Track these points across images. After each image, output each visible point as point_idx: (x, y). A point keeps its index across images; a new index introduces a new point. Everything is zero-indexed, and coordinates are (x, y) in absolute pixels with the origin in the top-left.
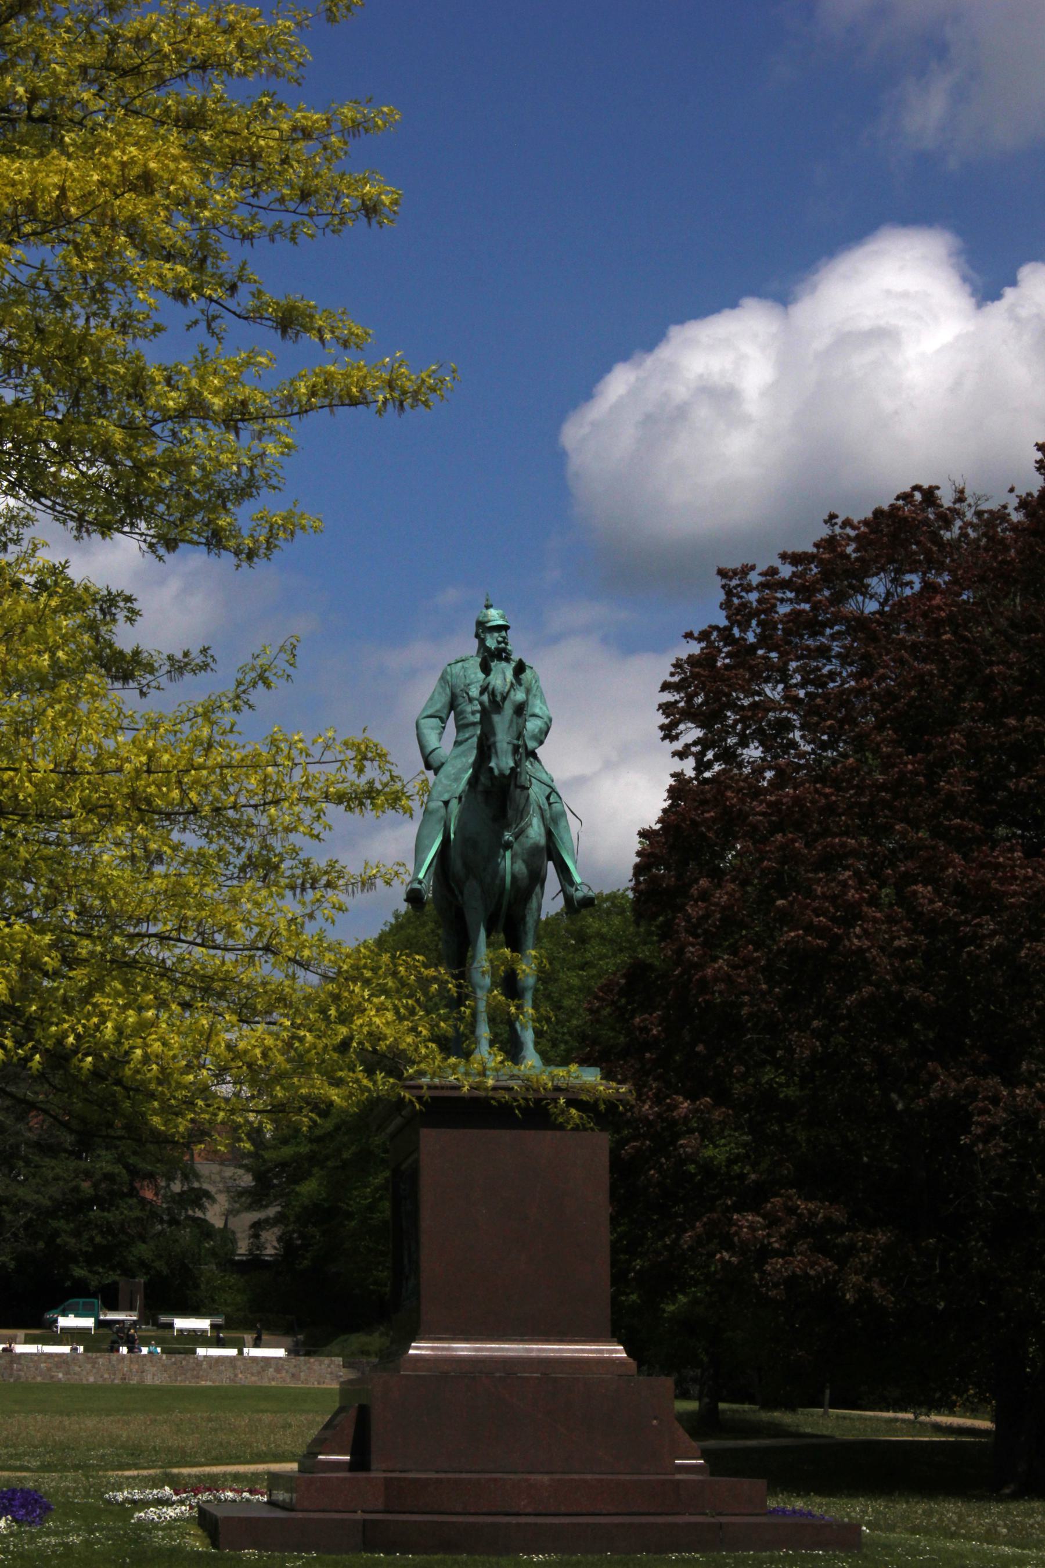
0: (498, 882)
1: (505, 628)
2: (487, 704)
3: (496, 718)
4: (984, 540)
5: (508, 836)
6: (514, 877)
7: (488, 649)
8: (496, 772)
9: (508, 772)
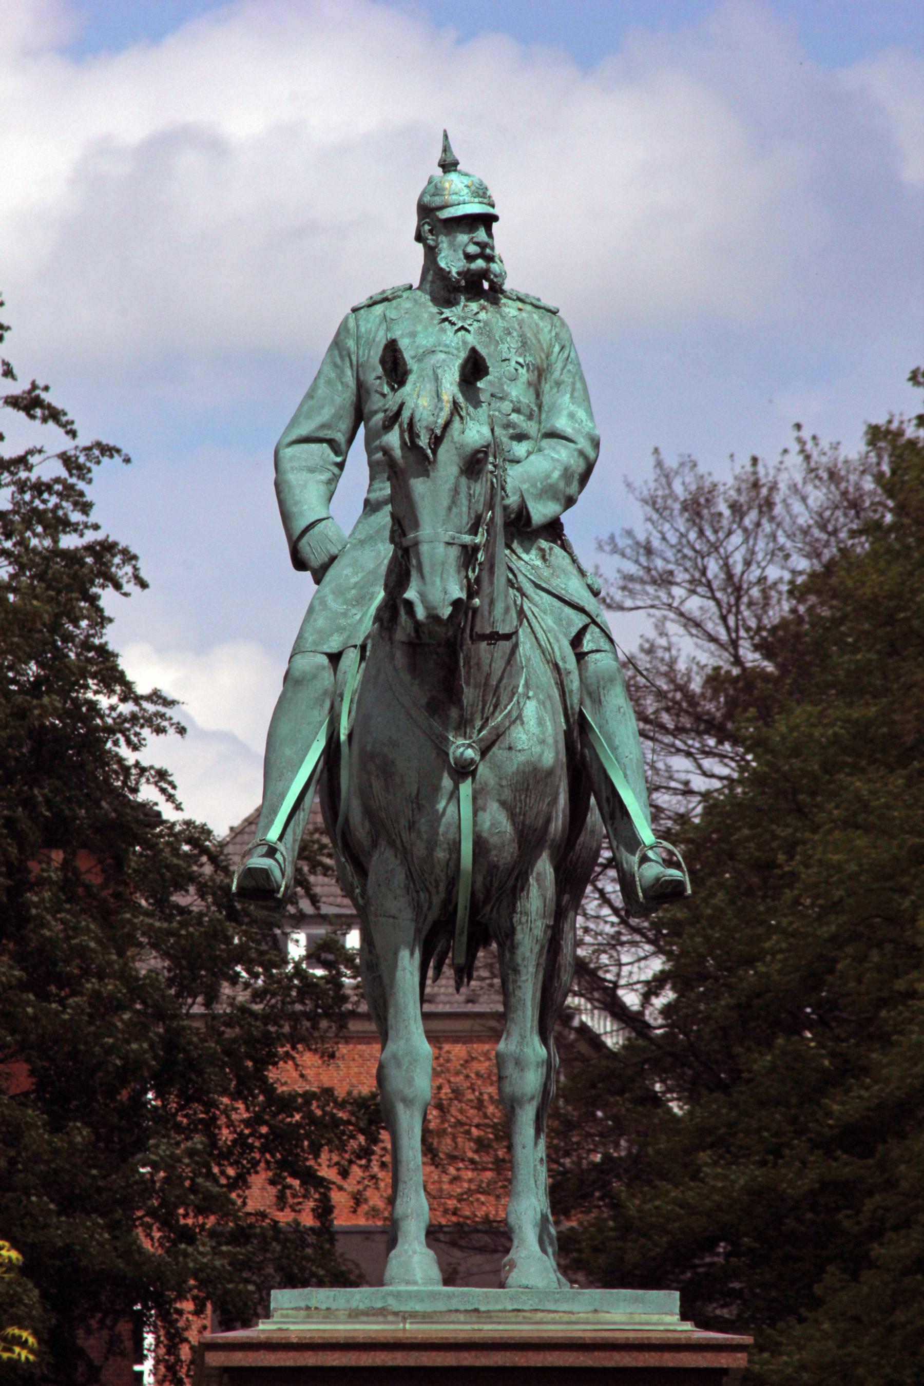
0: (441, 854)
1: (487, 221)
2: (398, 453)
3: (418, 486)
4: (67, 1178)
5: (462, 748)
6: (479, 843)
7: (442, 275)
8: (421, 613)
9: (446, 612)
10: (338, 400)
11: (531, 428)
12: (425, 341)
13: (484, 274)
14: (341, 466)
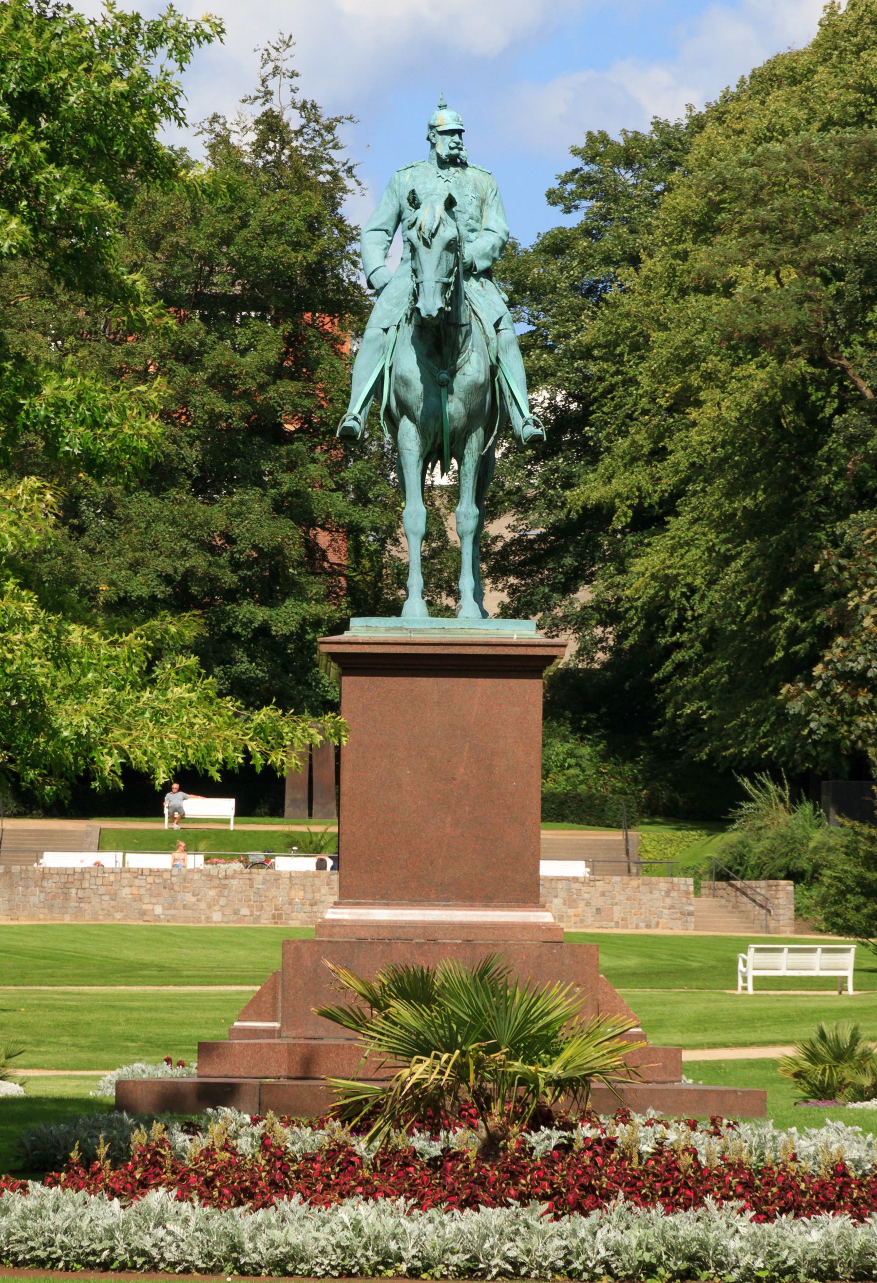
1: (459, 132)
12: (430, 186)
13: (457, 156)
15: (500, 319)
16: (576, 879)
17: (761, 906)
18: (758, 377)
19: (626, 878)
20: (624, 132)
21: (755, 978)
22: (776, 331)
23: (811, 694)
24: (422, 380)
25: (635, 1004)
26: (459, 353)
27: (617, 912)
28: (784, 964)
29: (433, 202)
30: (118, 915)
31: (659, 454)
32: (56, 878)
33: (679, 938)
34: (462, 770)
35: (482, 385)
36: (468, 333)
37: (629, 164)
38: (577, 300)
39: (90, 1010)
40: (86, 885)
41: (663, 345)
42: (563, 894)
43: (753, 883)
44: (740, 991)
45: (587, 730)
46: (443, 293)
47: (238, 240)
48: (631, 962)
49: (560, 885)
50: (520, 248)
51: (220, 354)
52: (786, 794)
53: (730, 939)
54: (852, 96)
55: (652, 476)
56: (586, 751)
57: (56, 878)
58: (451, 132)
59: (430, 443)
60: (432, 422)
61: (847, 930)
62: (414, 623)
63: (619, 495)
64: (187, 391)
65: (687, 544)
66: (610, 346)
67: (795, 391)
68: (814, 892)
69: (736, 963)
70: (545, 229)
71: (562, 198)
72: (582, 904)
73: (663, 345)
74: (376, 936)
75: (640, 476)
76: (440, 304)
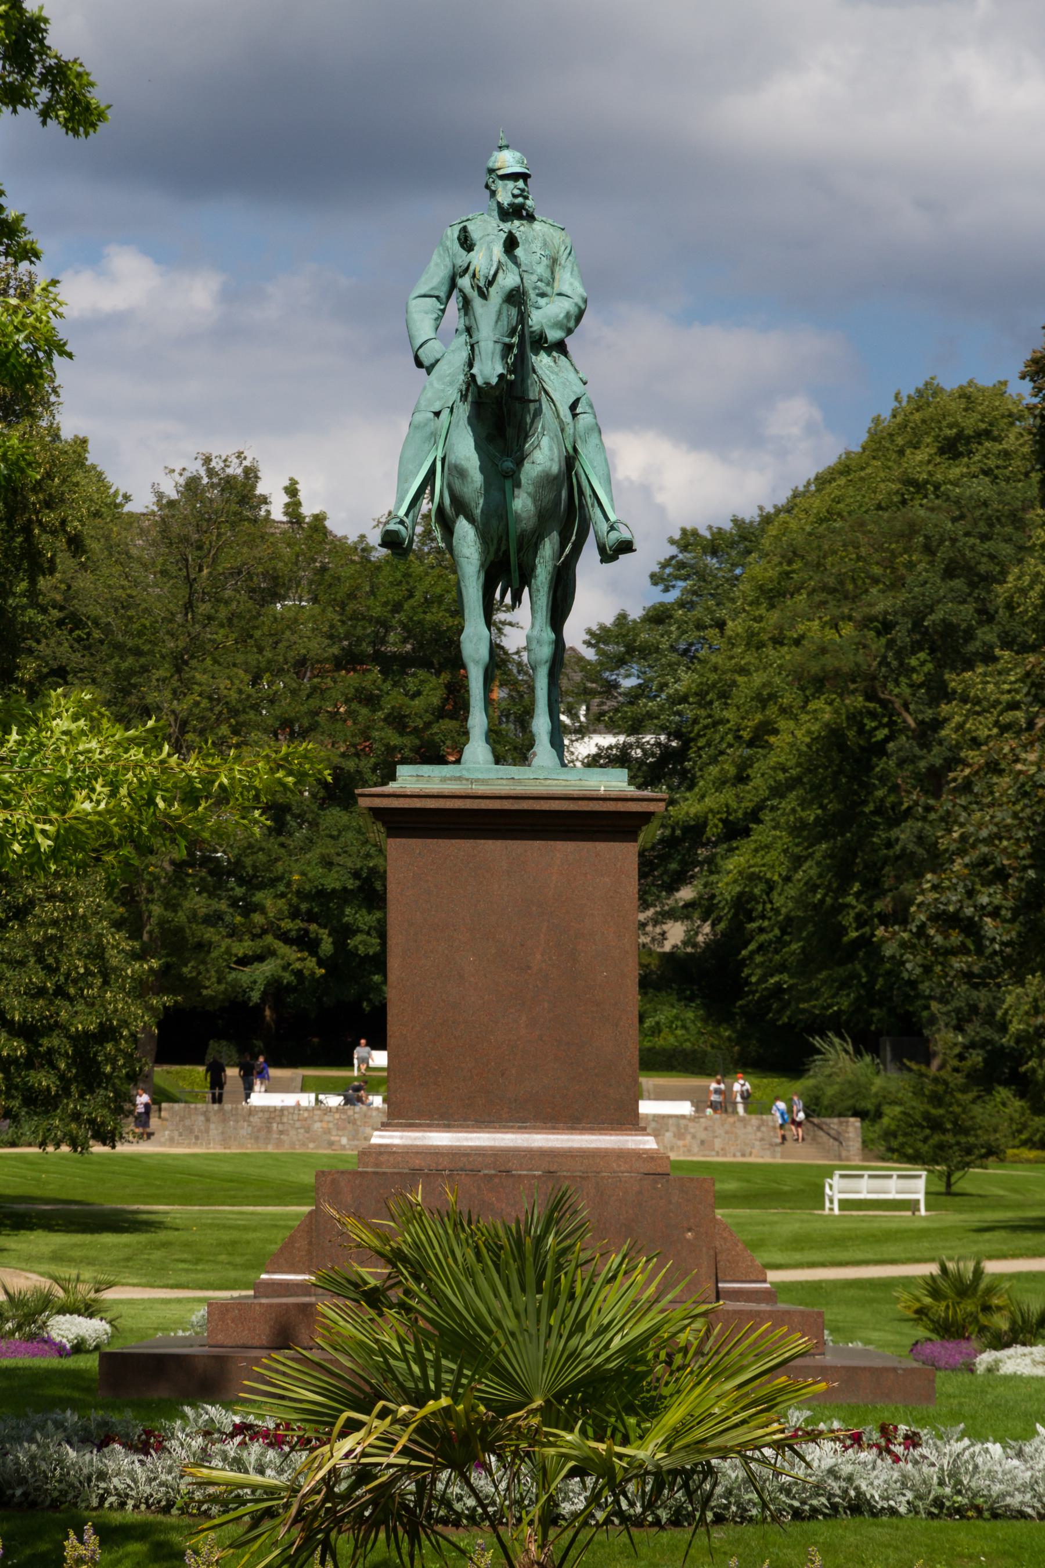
1: (525, 177)
10: (442, 274)
11: (548, 290)
13: (522, 206)
14: (443, 311)
15: (578, 400)
16: (683, 1117)
17: (835, 1139)
18: (824, 711)
19: (724, 1116)
20: (710, 528)
21: (841, 1201)
22: (837, 672)
23: (905, 935)
24: (482, 469)
25: (738, 1224)
26: (526, 437)
27: (718, 1144)
28: (865, 1188)
29: (489, 243)
30: (311, 1145)
31: (742, 779)
32: (261, 1115)
33: (770, 1165)
34: (539, 956)
35: (556, 478)
36: (538, 412)
37: (714, 553)
38: (674, 657)
39: (255, 1229)
40: (285, 1120)
41: (746, 687)
42: (673, 1129)
43: (828, 1120)
44: (827, 1212)
45: (691, 999)
46: (504, 356)
47: (406, 607)
48: (731, 1186)
49: (671, 1121)
50: (630, 618)
51: (393, 699)
52: (850, 1048)
53: (811, 1166)
54: (894, 487)
55: (737, 796)
56: (690, 1015)
57: (261, 1115)
58: (514, 177)
59: (493, 549)
60: (494, 522)
61: (915, 1159)
62: (476, 771)
63: (711, 810)
64: (368, 727)
65: (767, 846)
66: (701, 694)
67: (855, 718)
68: (877, 1127)
69: (824, 1187)
70: (648, 604)
71: (663, 579)
72: (689, 1137)
73: (746, 687)
74: (433, 1166)
75: (727, 796)
76: (500, 369)
